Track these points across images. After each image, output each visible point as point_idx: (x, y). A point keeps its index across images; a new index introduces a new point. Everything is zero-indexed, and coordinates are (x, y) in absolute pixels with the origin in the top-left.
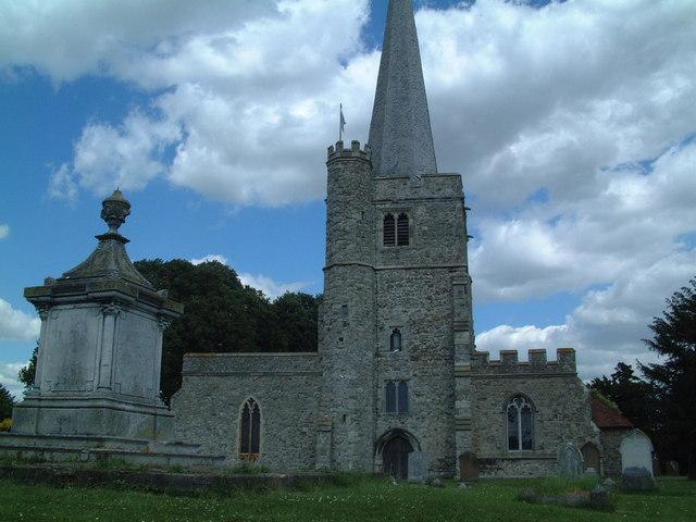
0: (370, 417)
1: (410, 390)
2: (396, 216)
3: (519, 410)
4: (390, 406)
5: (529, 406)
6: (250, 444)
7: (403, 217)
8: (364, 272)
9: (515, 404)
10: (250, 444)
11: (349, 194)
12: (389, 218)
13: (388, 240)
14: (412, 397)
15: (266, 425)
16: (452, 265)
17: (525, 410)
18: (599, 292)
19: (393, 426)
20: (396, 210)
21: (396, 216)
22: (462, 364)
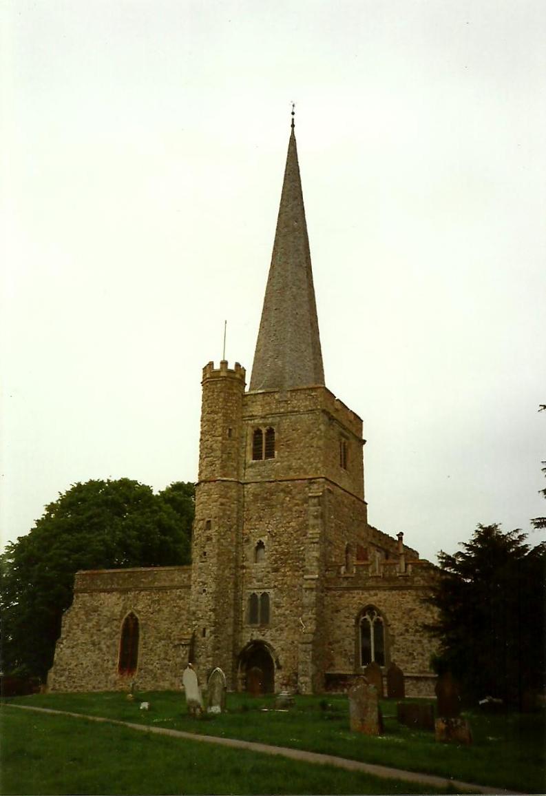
0: (230, 630)
1: (271, 602)
2: (264, 430)
3: (372, 623)
4: (253, 619)
5: (381, 618)
6: (128, 662)
7: (270, 432)
8: (228, 487)
9: (367, 617)
10: (128, 662)
11: (217, 413)
12: (258, 432)
13: (257, 456)
14: (272, 608)
15: (144, 638)
16: (310, 477)
17: (378, 623)
18: (62, 652)
19: (254, 638)
20: (265, 425)
21: (264, 430)
22: (402, 551)
